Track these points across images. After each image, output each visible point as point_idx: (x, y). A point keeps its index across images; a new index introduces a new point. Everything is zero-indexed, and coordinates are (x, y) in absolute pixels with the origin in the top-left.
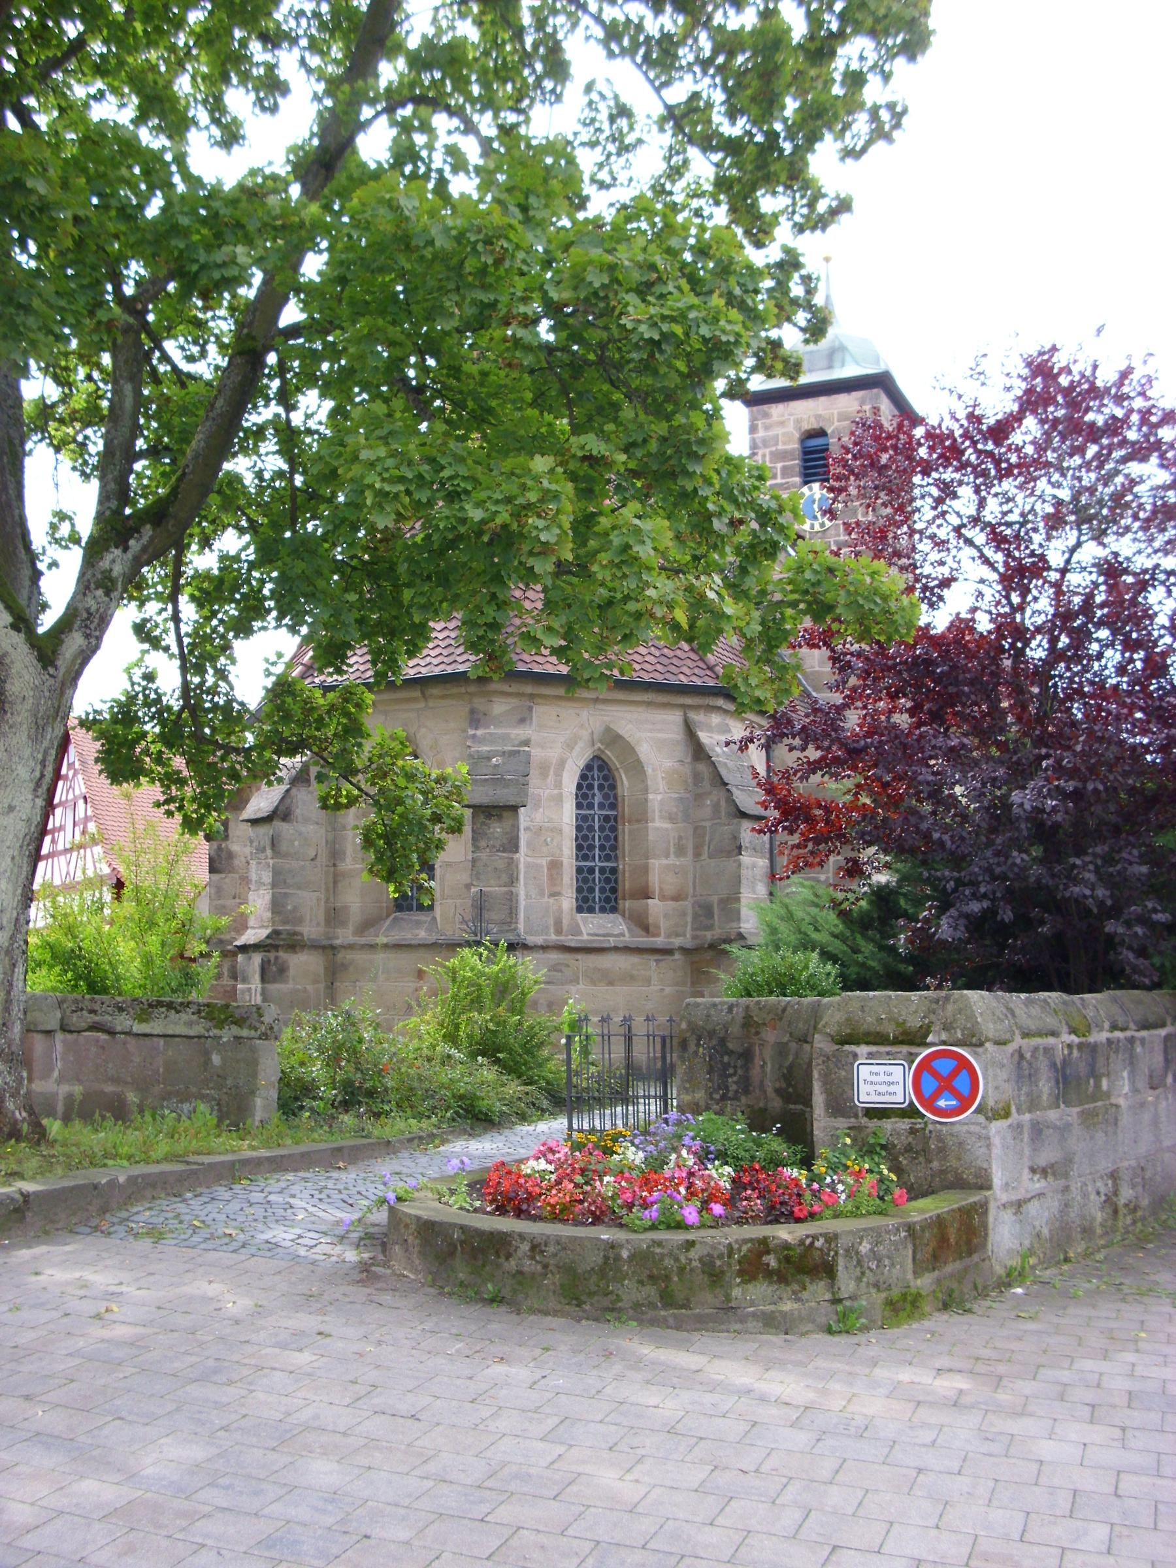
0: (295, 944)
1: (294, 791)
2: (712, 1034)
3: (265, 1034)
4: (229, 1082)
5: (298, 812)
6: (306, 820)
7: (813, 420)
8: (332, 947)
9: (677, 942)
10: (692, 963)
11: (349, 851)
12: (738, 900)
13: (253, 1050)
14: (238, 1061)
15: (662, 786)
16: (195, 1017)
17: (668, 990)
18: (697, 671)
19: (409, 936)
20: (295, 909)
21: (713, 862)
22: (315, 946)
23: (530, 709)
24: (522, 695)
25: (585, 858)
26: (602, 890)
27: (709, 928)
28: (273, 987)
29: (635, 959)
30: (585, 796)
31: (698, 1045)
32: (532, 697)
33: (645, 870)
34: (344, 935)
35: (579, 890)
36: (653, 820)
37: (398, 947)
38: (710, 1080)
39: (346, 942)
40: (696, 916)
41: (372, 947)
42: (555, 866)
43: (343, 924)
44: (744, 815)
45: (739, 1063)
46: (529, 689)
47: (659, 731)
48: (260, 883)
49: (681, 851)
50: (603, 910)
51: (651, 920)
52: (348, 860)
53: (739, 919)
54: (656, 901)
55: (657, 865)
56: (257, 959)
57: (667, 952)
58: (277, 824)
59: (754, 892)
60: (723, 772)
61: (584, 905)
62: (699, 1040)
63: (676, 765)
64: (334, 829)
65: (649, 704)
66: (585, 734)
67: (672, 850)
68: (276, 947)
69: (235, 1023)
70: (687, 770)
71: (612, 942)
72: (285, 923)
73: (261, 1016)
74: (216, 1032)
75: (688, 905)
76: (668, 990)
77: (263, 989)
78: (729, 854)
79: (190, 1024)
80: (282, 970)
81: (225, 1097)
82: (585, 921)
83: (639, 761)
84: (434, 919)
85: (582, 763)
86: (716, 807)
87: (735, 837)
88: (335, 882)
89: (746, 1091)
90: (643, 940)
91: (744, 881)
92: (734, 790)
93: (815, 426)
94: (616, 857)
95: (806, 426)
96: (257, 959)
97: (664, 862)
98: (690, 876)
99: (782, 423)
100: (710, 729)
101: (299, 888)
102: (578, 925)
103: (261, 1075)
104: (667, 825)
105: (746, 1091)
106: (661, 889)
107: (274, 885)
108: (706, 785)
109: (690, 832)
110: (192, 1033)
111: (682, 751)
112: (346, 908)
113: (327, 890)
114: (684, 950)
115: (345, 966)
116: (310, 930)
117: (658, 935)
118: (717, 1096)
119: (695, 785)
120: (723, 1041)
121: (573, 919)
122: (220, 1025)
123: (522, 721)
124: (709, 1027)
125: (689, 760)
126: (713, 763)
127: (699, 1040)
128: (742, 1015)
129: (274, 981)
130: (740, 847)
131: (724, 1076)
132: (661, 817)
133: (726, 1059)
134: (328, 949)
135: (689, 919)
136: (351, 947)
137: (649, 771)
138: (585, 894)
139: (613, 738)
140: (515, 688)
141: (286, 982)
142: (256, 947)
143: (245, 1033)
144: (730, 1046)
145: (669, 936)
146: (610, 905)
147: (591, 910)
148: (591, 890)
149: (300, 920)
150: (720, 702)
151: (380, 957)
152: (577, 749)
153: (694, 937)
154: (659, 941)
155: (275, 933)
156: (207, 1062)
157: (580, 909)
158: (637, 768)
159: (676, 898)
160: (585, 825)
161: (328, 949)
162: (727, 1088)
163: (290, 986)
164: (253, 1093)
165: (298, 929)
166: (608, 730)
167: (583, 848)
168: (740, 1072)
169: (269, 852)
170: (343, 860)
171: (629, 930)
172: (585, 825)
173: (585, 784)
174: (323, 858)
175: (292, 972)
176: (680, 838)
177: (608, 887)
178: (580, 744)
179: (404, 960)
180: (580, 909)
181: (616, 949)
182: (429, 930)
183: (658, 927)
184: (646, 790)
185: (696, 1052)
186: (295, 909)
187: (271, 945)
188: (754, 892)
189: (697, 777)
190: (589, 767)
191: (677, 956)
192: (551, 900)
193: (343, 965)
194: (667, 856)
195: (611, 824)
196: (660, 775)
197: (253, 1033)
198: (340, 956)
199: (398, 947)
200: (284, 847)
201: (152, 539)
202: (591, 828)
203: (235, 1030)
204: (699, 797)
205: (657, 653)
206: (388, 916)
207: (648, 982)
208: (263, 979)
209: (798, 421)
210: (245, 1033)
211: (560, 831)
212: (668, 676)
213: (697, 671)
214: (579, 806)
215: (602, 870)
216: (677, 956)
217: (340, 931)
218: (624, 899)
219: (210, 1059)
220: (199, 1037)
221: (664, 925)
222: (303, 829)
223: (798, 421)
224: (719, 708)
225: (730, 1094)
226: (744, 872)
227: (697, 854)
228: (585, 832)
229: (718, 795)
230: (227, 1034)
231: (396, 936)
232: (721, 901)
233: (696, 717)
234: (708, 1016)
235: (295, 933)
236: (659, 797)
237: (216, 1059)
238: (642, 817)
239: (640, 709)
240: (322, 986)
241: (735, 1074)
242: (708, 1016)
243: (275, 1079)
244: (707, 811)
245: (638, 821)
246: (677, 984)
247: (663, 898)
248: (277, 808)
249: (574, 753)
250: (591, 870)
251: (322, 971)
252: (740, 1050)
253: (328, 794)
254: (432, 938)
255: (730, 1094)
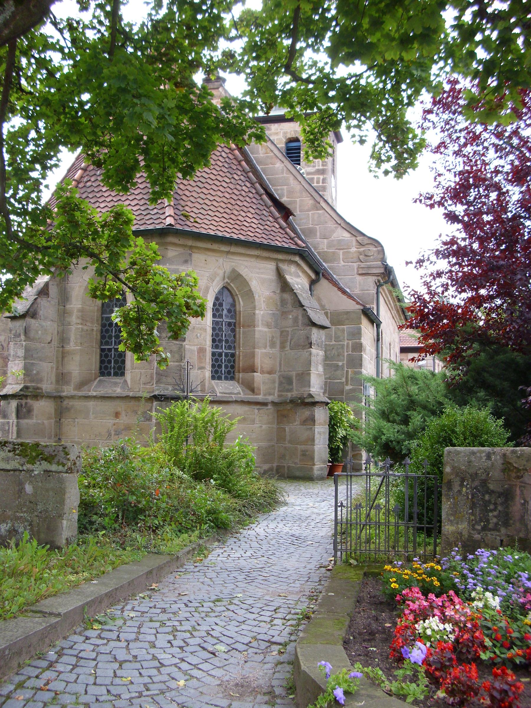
0: (37, 395)
1: (39, 300)
2: (474, 476)
3: (70, 469)
4: (40, 507)
5: (41, 313)
6: (46, 318)
7: (293, 133)
8: (61, 397)
9: (270, 398)
10: (278, 411)
11: (72, 338)
12: (309, 374)
13: (61, 481)
14: (47, 490)
15: (263, 306)
16: (11, 454)
17: (264, 427)
18: (284, 239)
19: (110, 391)
20: (38, 373)
21: (293, 352)
22: (49, 397)
23: (190, 255)
24: (184, 246)
25: (217, 347)
26: (226, 367)
27: (290, 390)
28: (24, 422)
29: (246, 408)
30: (217, 310)
31: (462, 485)
32: (191, 247)
33: (253, 355)
34: (68, 390)
35: (213, 366)
36: (258, 326)
37: (103, 398)
38: (472, 514)
39: (69, 394)
40: (281, 383)
41: (87, 398)
42: (201, 351)
43: (67, 383)
44: (314, 325)
45: (500, 500)
46: (190, 243)
47: (262, 273)
48: (16, 357)
49: (273, 345)
50: (226, 378)
51: (255, 385)
52: (72, 344)
53: (309, 386)
54: (258, 374)
55: (259, 352)
56: (14, 404)
57: (265, 404)
58: (28, 320)
59: (317, 370)
60: (301, 299)
61: (216, 375)
62: (463, 480)
63: (272, 294)
64: (63, 325)
65: (257, 257)
66: (221, 272)
67: (268, 344)
68: (26, 397)
69: (46, 460)
70: (277, 297)
71: (234, 398)
72: (31, 381)
73: (67, 454)
74: (29, 466)
75: (276, 376)
76: (264, 427)
77: (18, 423)
78: (304, 347)
79: (7, 460)
80: (30, 411)
81: (36, 520)
82: (217, 385)
83: (250, 290)
84: (126, 381)
85: (217, 290)
86: (296, 320)
87: (308, 338)
88: (63, 358)
89: (506, 524)
90: (251, 397)
91: (312, 363)
92: (307, 309)
93: (294, 136)
94: (235, 347)
95: (289, 136)
96: (14, 404)
97: (264, 351)
98: (278, 360)
99: (277, 134)
100: (291, 274)
101: (41, 360)
102: (213, 387)
103: (67, 501)
104: (266, 329)
105: (506, 524)
106: (262, 367)
107: (25, 358)
108: (289, 307)
109: (278, 334)
110: (8, 467)
111: (275, 286)
112: (70, 373)
113: (58, 362)
114: (273, 403)
115: (68, 409)
116: (47, 386)
117: (259, 394)
118: (479, 528)
119: (282, 306)
120: (484, 483)
121: (210, 383)
122: (32, 461)
123: (186, 262)
124: (471, 471)
125: (278, 292)
126: (295, 293)
127: (463, 480)
128: (500, 461)
129: (25, 418)
130: (311, 343)
131: (485, 510)
132: (263, 324)
133: (487, 497)
134: (58, 398)
135: (277, 385)
136: (72, 397)
137: (256, 297)
138: (216, 368)
139: (236, 276)
140: (182, 241)
141: (32, 418)
142: (14, 396)
143: (54, 467)
144: (491, 487)
145: (265, 395)
146: (231, 376)
147: (219, 378)
148: (220, 366)
149: (41, 380)
150: (297, 259)
151: (91, 404)
152: (215, 282)
153: (279, 396)
154: (260, 398)
155: (26, 388)
156: (21, 490)
157: (213, 378)
158: (249, 294)
159: (270, 373)
160: (217, 327)
161: (58, 398)
162: (488, 521)
163: (34, 421)
164: (60, 516)
165: (39, 385)
166: (234, 271)
167: (216, 341)
168: (499, 508)
169: (23, 337)
170: (69, 343)
171: (242, 390)
172: (217, 327)
173: (217, 303)
174: (55, 343)
175: (35, 412)
176: (273, 337)
177: (229, 365)
178: (218, 279)
179: (109, 406)
180: (213, 378)
181: (236, 402)
182: (123, 388)
183: (259, 389)
184: (254, 308)
185: (460, 492)
186: (38, 373)
187: (23, 395)
188: (317, 371)
189: (283, 302)
190: (221, 292)
191: (270, 407)
192: (199, 372)
193: (66, 408)
194: (265, 348)
195: (233, 327)
196: (262, 299)
197: (61, 468)
198: (65, 403)
199: (103, 398)
200: (32, 334)
201: (13, 15)
202: (221, 329)
203: (45, 465)
204: (284, 314)
205: (262, 228)
206: (95, 379)
207: (253, 422)
208: (18, 417)
209: (285, 133)
210: (54, 467)
211: (205, 330)
212: (269, 241)
213: (284, 239)
214: (214, 316)
215: (226, 355)
216: (270, 407)
217: (65, 388)
218: (239, 372)
219: (23, 488)
220: (14, 470)
221: (263, 388)
222: (44, 324)
223: (285, 133)
224: (296, 263)
225: (491, 526)
226: (313, 358)
227: (282, 347)
228: (217, 331)
229: (300, 312)
230: (38, 468)
231: (101, 391)
232: (298, 375)
233: (284, 267)
234: (470, 462)
235: (38, 388)
236: (262, 313)
237: (29, 488)
238: (251, 324)
239: (252, 260)
240: (53, 421)
241: (495, 510)
242: (470, 462)
243: (77, 503)
244: (290, 322)
245: (249, 326)
246: (269, 423)
247: (262, 372)
248: (29, 309)
249: (214, 283)
250: (220, 355)
251: (53, 411)
252: (500, 490)
253: (96, 288)
254: (125, 393)
255: (491, 526)
